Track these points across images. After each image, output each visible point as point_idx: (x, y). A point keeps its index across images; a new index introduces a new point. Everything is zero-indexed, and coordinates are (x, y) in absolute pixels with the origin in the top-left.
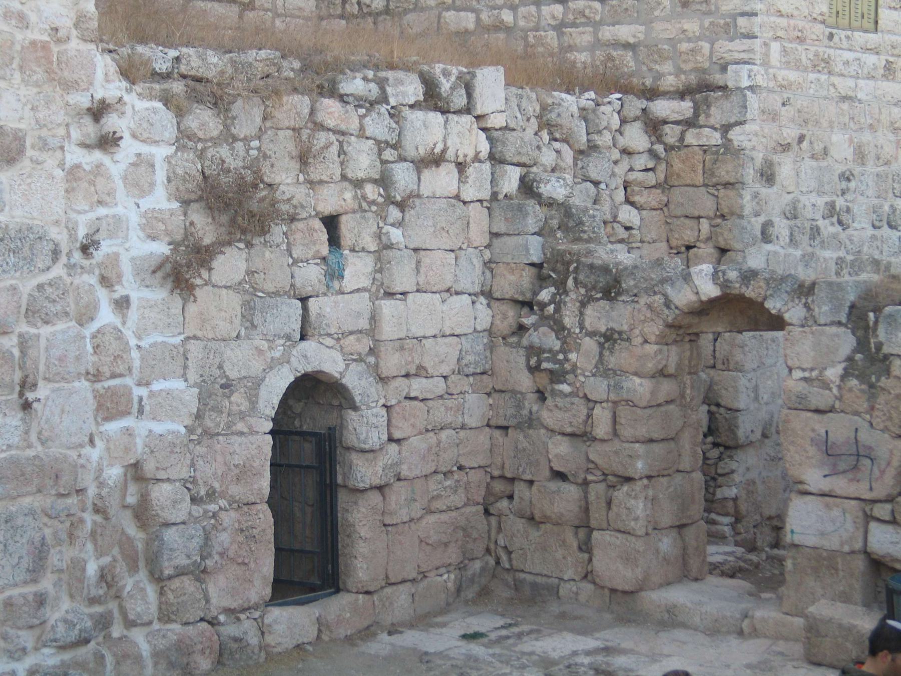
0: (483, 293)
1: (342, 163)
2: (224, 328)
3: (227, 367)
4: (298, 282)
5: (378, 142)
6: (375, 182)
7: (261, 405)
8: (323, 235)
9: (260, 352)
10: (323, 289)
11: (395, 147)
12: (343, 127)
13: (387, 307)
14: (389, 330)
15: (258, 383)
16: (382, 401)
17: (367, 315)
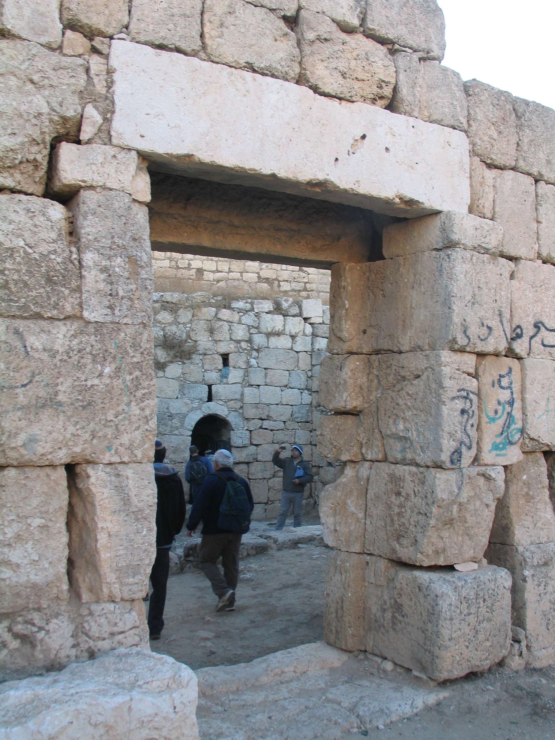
0: (307, 389)
1: (230, 334)
2: (170, 394)
3: (171, 409)
4: (206, 378)
5: (248, 326)
6: (246, 341)
7: (186, 424)
8: (221, 361)
9: (187, 404)
10: (219, 382)
11: (256, 328)
12: (231, 320)
13: (247, 390)
14: (247, 399)
15: (185, 416)
16: (246, 428)
17: (240, 393)
